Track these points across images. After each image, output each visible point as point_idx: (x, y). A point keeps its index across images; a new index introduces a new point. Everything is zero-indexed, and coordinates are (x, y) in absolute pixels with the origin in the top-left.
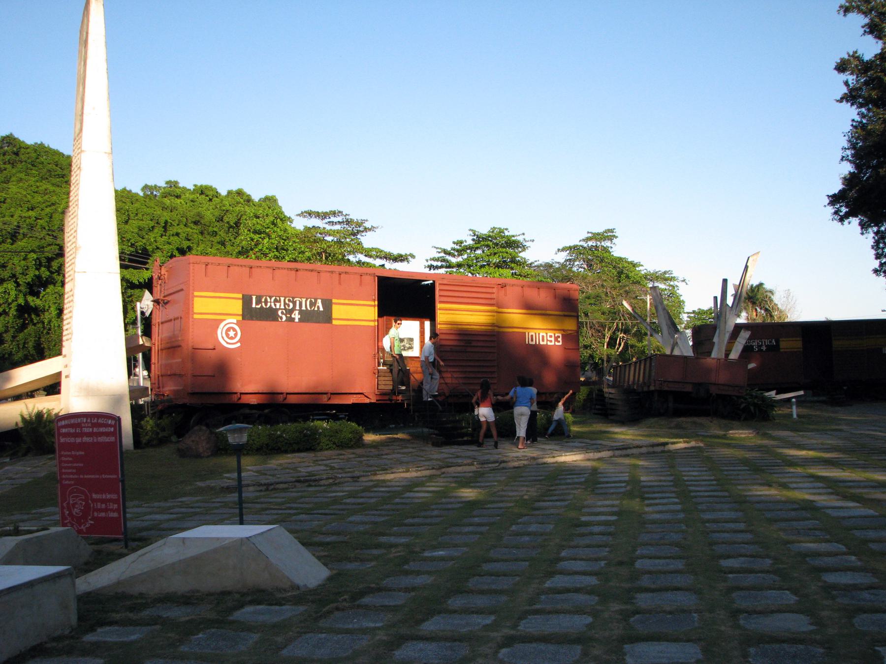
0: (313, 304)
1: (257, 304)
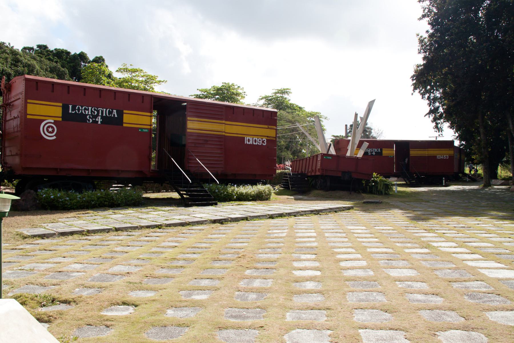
0: (110, 113)
1: (72, 111)
